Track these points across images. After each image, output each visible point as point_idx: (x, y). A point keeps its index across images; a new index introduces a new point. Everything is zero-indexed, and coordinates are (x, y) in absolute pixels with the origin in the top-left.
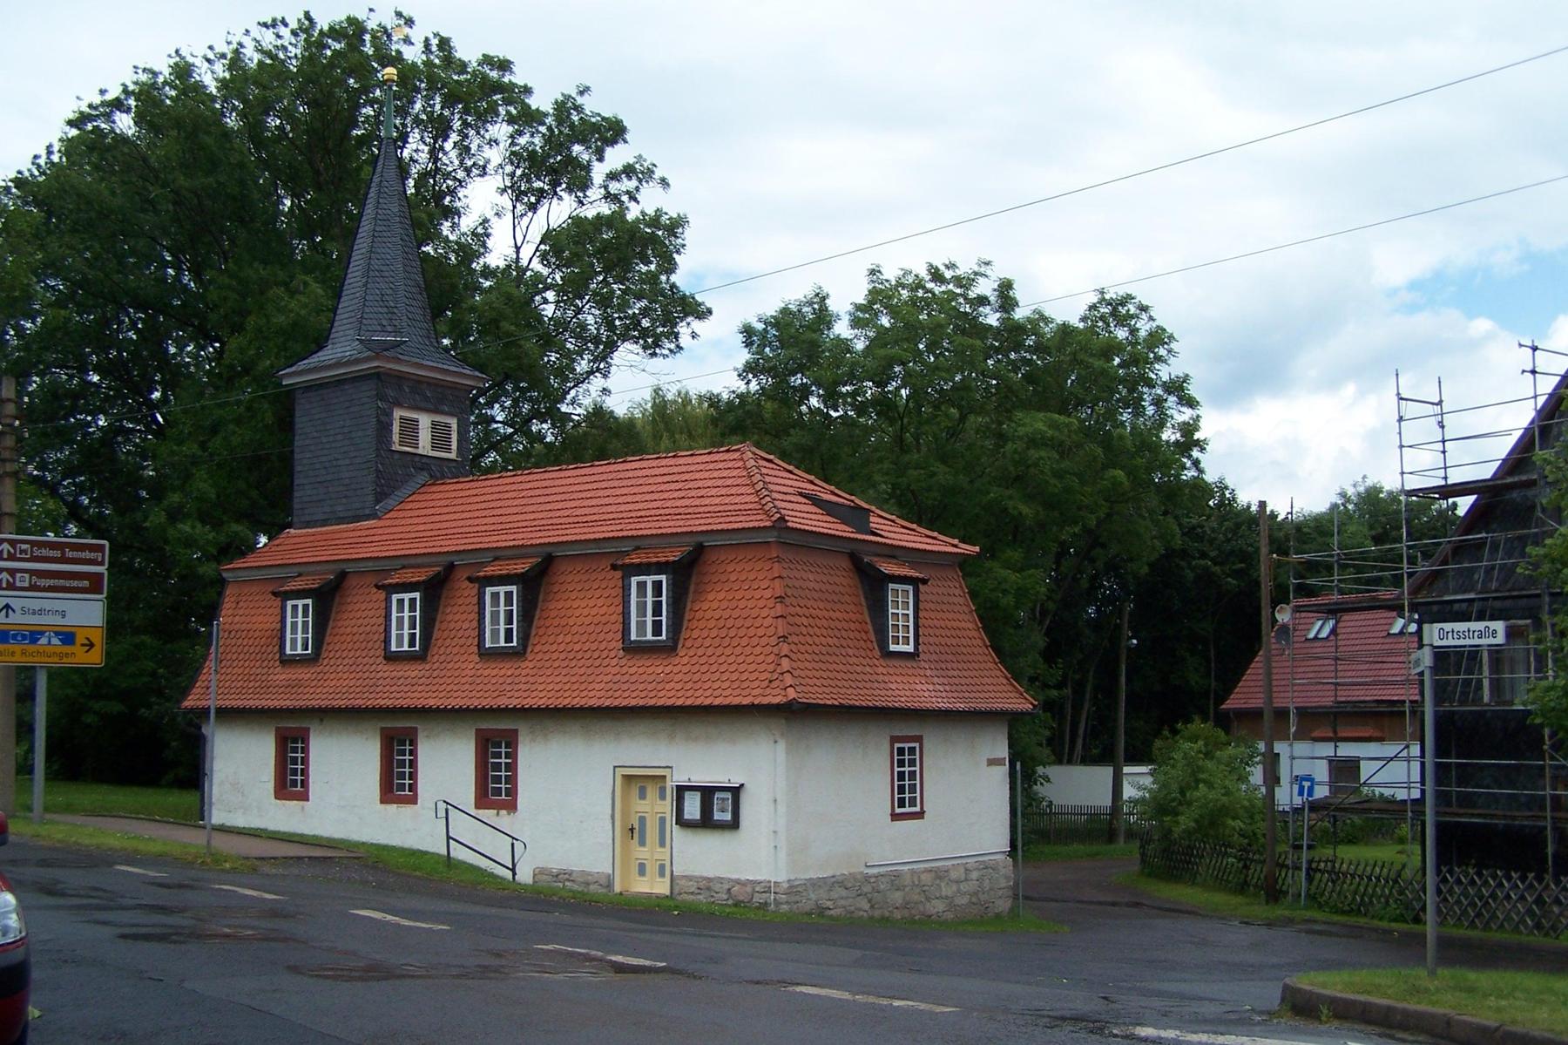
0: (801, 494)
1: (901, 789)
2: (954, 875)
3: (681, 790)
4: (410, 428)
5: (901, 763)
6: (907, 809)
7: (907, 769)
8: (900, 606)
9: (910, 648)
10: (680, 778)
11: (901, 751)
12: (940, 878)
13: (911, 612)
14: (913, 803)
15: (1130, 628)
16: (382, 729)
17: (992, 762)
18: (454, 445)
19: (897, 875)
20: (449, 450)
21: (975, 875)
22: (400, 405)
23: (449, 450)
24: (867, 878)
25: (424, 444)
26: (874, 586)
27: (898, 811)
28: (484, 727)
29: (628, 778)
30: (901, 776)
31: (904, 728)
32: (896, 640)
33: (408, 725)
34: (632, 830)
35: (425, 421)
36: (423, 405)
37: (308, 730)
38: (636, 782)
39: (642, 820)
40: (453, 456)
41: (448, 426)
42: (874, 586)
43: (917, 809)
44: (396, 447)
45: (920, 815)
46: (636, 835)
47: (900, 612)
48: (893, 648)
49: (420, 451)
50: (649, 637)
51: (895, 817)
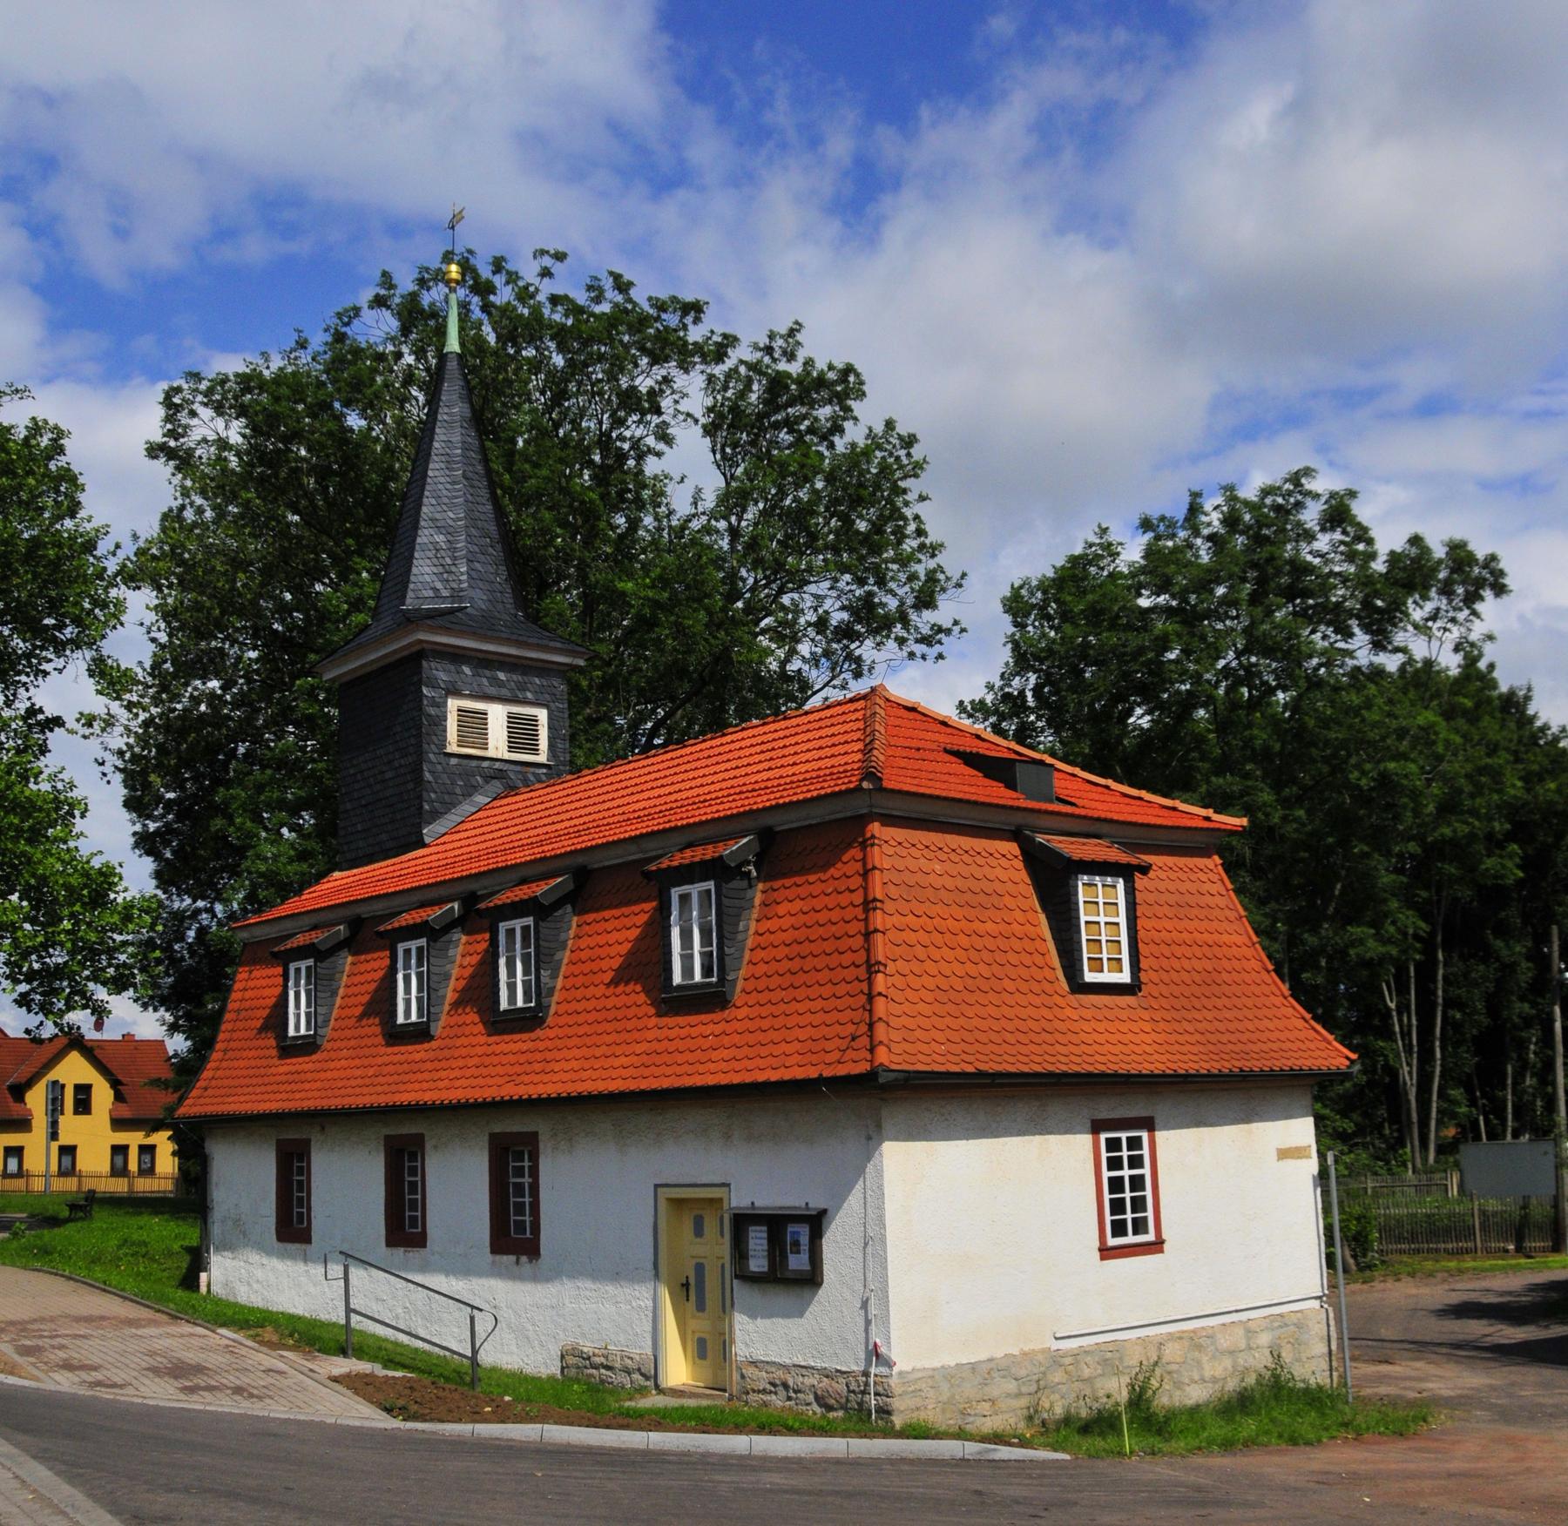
0: (946, 751)
1: (1118, 1207)
2: (1224, 1342)
3: (742, 1222)
4: (474, 724)
5: (1115, 1164)
6: (1131, 1239)
7: (1126, 1173)
8: (1101, 907)
9: (1125, 977)
10: (740, 1199)
11: (1113, 1145)
12: (1199, 1347)
13: (1122, 919)
14: (1140, 1226)
15: (1561, 959)
16: (388, 1138)
17: (1284, 1154)
18: (543, 743)
19: (1118, 1348)
20: (535, 751)
21: (1264, 1339)
22: (457, 693)
23: (535, 751)
24: (1056, 1359)
25: (497, 744)
26: (1054, 882)
27: (1113, 1242)
28: (497, 1130)
29: (678, 1204)
30: (1116, 1185)
31: (1121, 1104)
32: (1097, 965)
33: (414, 1131)
34: (686, 1285)
35: (497, 715)
36: (492, 691)
37: (307, 1143)
38: (687, 1206)
39: (700, 1268)
40: (542, 758)
41: (534, 720)
42: (1054, 882)
43: (1150, 1237)
44: (453, 747)
45: (1157, 1246)
46: (693, 1297)
47: (1102, 919)
48: (1090, 977)
49: (491, 753)
50: (698, 977)
51: (1106, 1252)
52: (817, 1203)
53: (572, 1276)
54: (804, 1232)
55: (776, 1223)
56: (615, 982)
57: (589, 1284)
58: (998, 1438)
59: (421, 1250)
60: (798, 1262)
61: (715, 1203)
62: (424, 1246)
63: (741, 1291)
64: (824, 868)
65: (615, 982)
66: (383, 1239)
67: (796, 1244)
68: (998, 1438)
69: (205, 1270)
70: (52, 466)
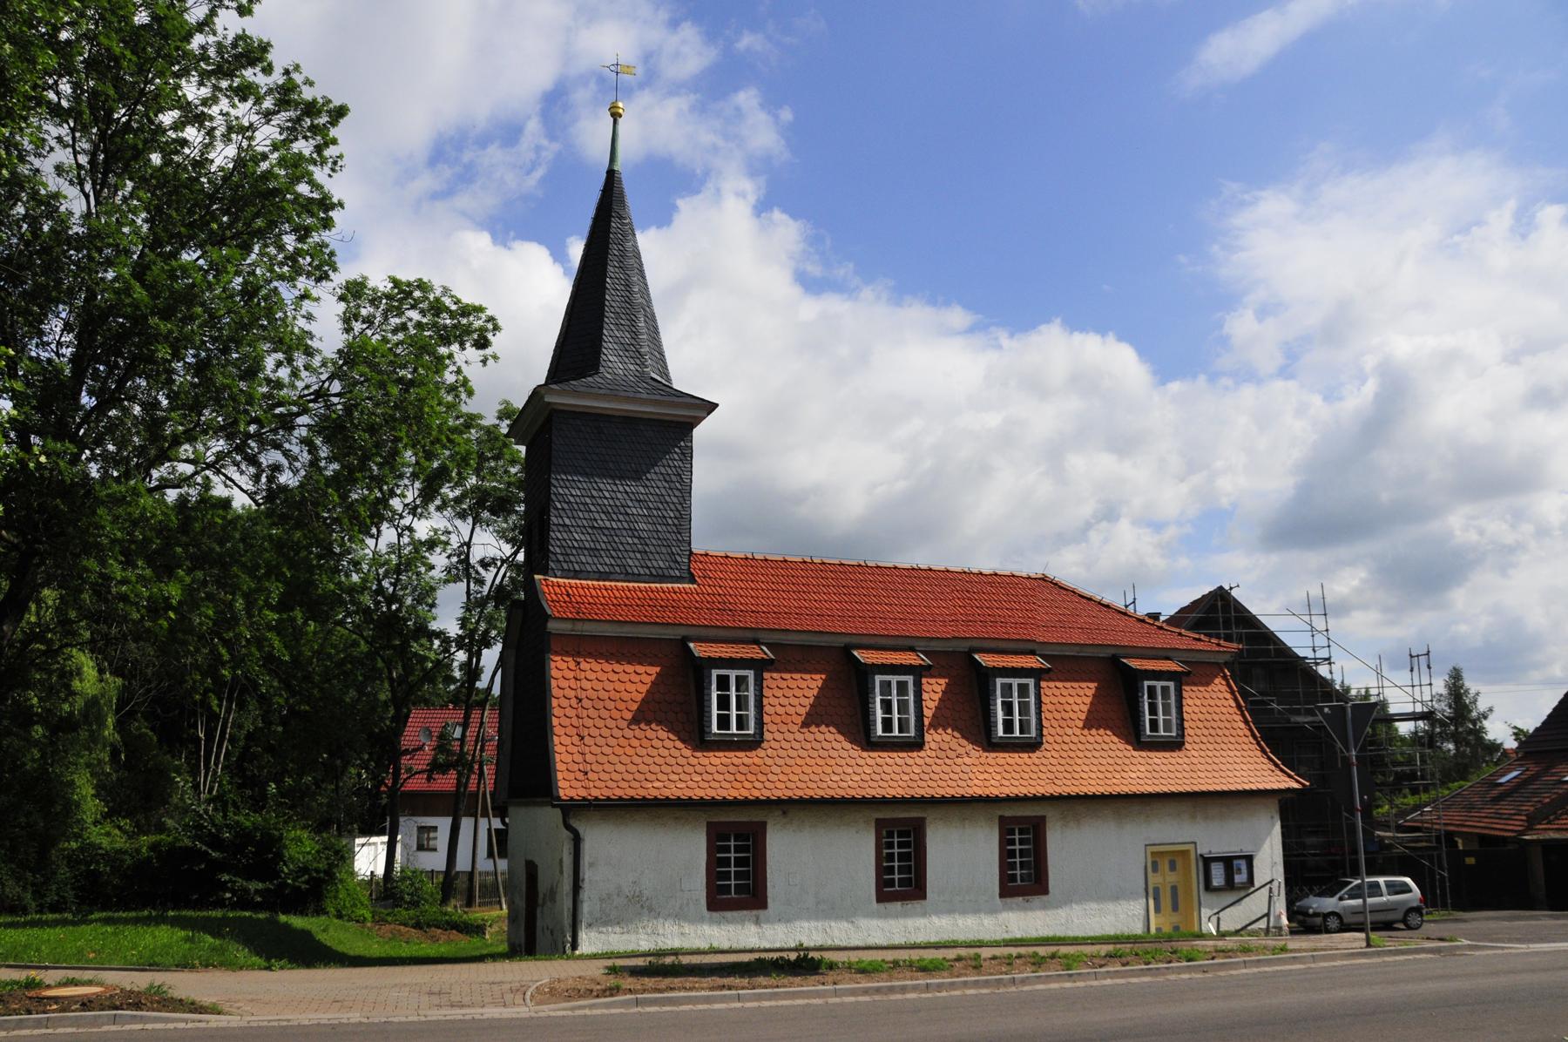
3: (1207, 862)
10: (1203, 849)
28: (716, 820)
52: (1247, 850)
53: (1079, 902)
54: (1243, 864)
55: (1228, 862)
56: (805, 724)
57: (1094, 906)
58: (1353, 955)
59: (1044, 898)
60: (1240, 878)
61: (1185, 853)
62: (924, 897)
63: (1205, 897)
64: (1208, 684)
65: (805, 724)
66: (703, 901)
67: (1239, 870)
68: (1353, 955)
69: (1433, 898)
70: (77, 230)
